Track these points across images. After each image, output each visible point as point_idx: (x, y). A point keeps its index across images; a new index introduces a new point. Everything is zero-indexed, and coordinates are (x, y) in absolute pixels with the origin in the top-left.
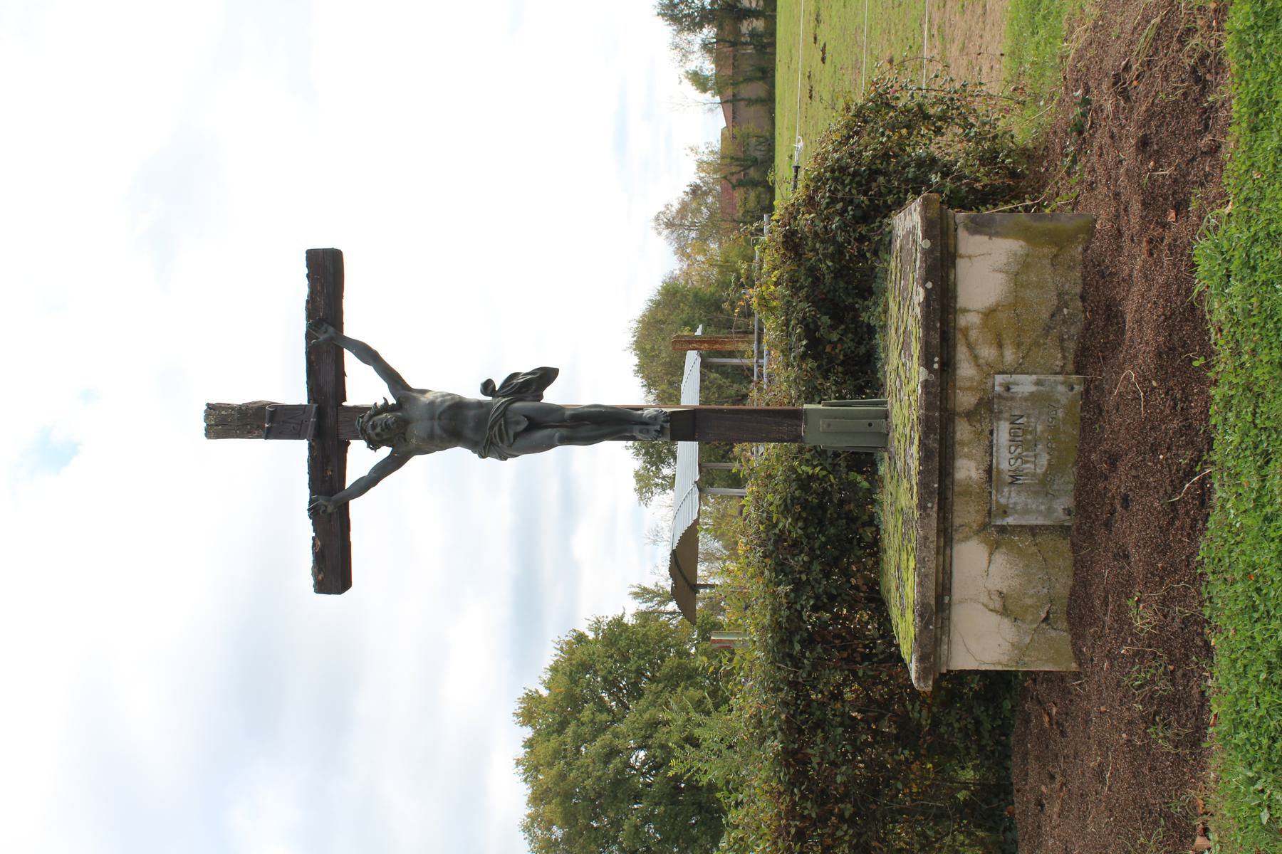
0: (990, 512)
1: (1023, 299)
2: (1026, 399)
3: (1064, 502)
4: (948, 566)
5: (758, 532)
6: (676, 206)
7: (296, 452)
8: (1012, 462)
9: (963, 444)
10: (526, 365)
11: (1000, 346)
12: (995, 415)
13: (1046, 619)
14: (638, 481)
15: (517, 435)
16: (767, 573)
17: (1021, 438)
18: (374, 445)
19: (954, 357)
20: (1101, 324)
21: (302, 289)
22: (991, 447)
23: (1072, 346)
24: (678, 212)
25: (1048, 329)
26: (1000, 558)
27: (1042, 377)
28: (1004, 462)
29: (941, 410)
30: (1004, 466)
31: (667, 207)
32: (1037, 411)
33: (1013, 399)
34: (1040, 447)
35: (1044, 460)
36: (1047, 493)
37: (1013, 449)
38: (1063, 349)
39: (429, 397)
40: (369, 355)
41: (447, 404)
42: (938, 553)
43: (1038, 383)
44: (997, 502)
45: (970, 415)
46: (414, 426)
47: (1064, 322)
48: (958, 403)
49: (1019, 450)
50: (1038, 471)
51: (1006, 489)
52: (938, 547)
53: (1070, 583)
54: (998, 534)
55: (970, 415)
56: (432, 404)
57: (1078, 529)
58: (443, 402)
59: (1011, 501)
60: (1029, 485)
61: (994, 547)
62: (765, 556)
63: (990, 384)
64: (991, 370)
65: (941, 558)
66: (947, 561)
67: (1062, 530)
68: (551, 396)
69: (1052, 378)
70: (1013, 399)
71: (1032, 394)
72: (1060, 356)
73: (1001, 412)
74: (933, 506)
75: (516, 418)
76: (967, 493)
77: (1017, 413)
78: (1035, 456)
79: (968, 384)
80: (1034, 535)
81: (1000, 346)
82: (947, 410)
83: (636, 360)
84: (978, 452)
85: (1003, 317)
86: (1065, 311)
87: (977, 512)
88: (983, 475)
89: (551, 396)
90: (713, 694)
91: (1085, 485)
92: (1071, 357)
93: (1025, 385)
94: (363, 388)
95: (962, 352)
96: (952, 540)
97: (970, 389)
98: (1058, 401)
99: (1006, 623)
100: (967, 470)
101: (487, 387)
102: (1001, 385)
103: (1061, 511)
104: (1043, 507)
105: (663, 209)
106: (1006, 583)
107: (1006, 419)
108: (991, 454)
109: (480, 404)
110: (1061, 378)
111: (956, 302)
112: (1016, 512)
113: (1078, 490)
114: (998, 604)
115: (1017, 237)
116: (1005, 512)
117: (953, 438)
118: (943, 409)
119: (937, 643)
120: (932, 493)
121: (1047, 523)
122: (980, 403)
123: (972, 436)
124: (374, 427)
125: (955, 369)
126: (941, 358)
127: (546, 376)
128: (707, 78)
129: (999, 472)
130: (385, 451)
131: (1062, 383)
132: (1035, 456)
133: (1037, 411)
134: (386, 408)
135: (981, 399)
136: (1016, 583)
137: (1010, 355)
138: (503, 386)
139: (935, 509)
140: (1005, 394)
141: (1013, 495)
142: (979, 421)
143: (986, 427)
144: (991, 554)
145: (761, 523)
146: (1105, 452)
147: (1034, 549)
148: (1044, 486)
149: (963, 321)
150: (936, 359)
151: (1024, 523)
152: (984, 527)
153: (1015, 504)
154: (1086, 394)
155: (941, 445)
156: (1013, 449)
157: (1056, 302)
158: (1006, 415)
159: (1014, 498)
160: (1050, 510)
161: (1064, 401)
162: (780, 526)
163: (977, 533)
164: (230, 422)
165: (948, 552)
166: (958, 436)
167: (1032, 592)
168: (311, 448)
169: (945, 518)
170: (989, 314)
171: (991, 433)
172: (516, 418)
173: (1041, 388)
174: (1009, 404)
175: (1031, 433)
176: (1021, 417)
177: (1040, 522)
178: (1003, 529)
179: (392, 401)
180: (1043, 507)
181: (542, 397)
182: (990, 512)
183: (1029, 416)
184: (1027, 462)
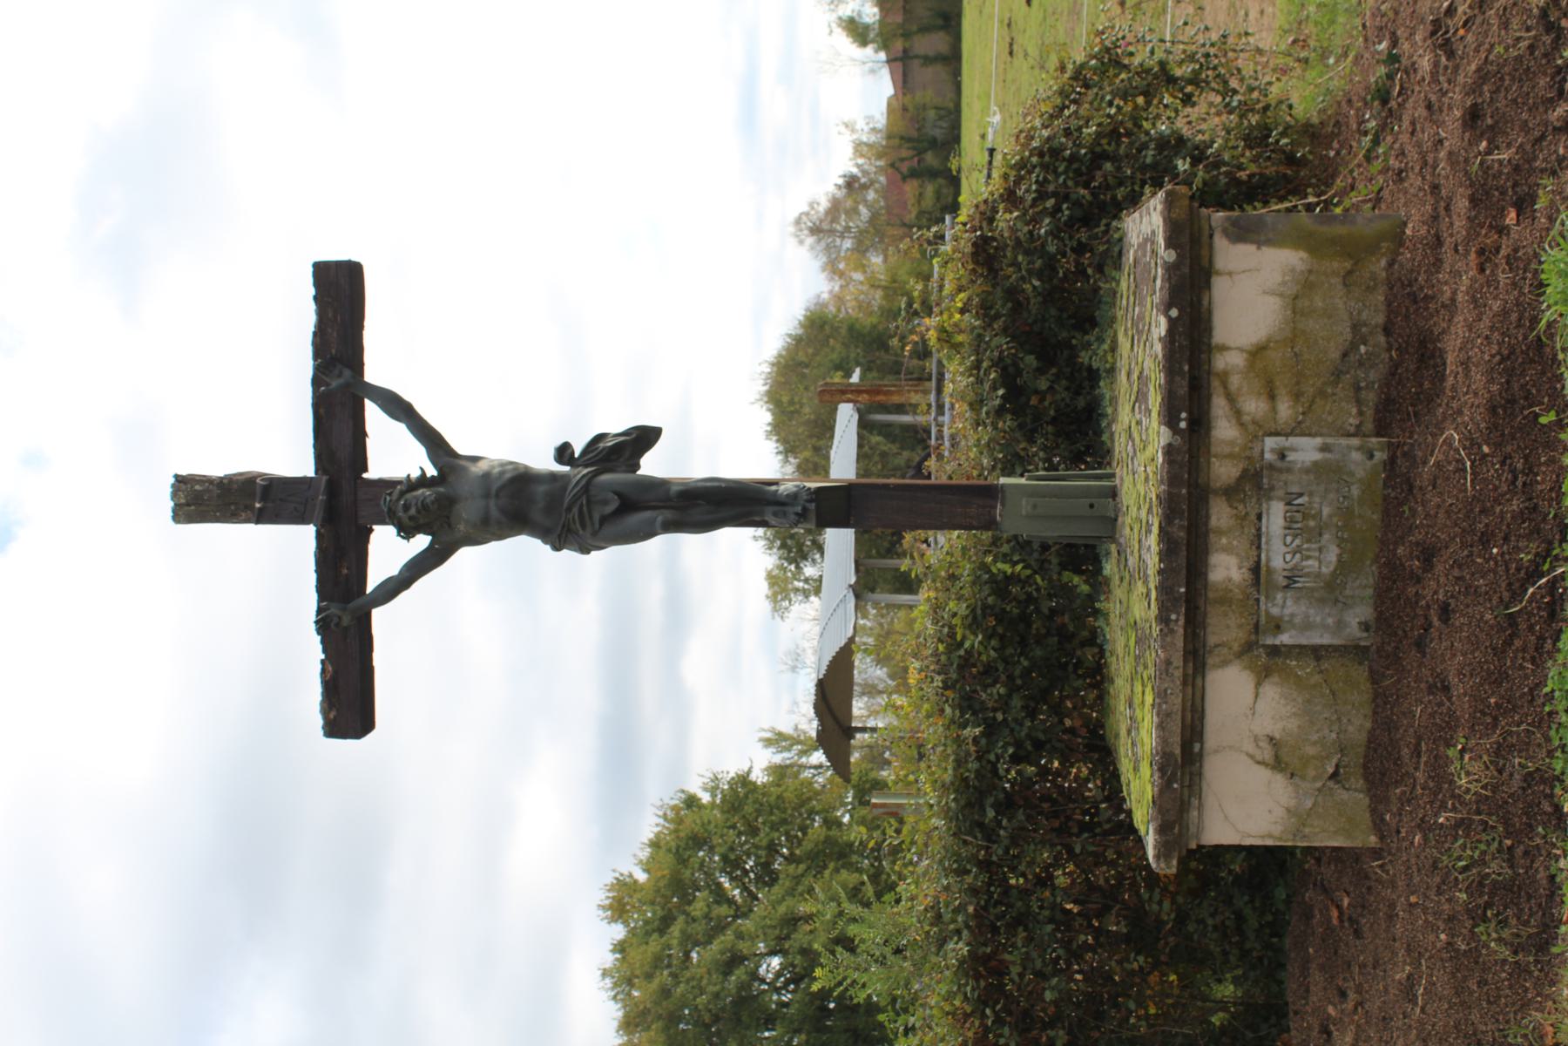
0: (1257, 626)
2: (1307, 471)
3: (1358, 615)
4: (1198, 701)
5: (936, 654)
6: (824, 204)
8: (1288, 557)
9: (1220, 532)
10: (616, 423)
11: (1272, 397)
14: (772, 585)
15: (604, 520)
16: (948, 710)
18: (407, 532)
19: (1208, 412)
20: (1412, 367)
21: (306, 316)
22: (1259, 536)
23: (1371, 397)
24: (828, 212)
25: (1337, 374)
26: (1271, 691)
27: (1329, 440)
28: (1278, 557)
29: (1189, 486)
30: (1277, 563)
31: (811, 205)
32: (1322, 487)
33: (1289, 470)
34: (1326, 536)
35: (1332, 555)
37: (1289, 539)
38: (1359, 402)
39: (482, 467)
40: (399, 408)
41: (508, 476)
42: (1184, 683)
43: (1325, 448)
44: (1267, 612)
45: (1231, 493)
46: (464, 505)
48: (1212, 476)
49: (1297, 542)
50: (1324, 570)
51: (1279, 596)
52: (1185, 675)
53: (1368, 725)
54: (1268, 658)
55: (1231, 493)
56: (486, 476)
57: (1378, 651)
58: (502, 473)
60: (1312, 590)
62: (946, 687)
63: (1257, 450)
64: (1258, 430)
66: (1198, 694)
68: (652, 465)
69: (1344, 441)
70: (1289, 470)
71: (1315, 463)
72: (1354, 411)
73: (1272, 488)
74: (1178, 619)
75: (602, 496)
76: (1225, 600)
77: (1295, 489)
78: (1320, 550)
79: (1227, 450)
80: (1318, 659)
81: (1272, 397)
83: (768, 417)
84: (1241, 543)
86: (1363, 349)
87: (1240, 626)
88: (1248, 575)
89: (652, 465)
91: (1389, 589)
92: (1369, 413)
93: (1306, 451)
94: (392, 454)
95: (1219, 405)
96: (1204, 665)
97: (1231, 456)
98: (1352, 474)
100: (1226, 568)
101: (563, 453)
102: (1272, 450)
105: (806, 209)
106: (1280, 726)
107: (1281, 499)
108: (1259, 547)
109: (553, 477)
110: (1355, 441)
112: (1294, 626)
117: (1206, 524)
121: (1336, 642)
122: (1244, 475)
123: (1232, 522)
124: (406, 507)
125: (1209, 429)
126: (1190, 413)
127: (645, 437)
128: (867, 27)
129: (1270, 571)
130: (422, 541)
131: (1359, 449)
132: (1320, 550)
133: (1322, 487)
134: (423, 481)
135: (1245, 471)
136: (1293, 725)
138: (585, 452)
139: (1182, 622)
140: (1279, 464)
141: (1289, 603)
142: (1243, 501)
144: (1258, 684)
145: (940, 641)
146: (1417, 544)
147: (1317, 678)
148: (1331, 591)
150: (1184, 415)
151: (1304, 642)
152: (1248, 648)
153: (1292, 615)
154: (1391, 463)
155: (1189, 533)
156: (1289, 539)
157: (1349, 337)
158: (1280, 493)
160: (1340, 625)
161: (1360, 473)
162: (967, 645)
163: (1239, 655)
164: (206, 500)
165: (1199, 681)
166: (1213, 522)
167: (1315, 737)
169: (1195, 635)
171: (1259, 517)
172: (602, 496)
173: (1328, 456)
174: (1284, 477)
175: (1314, 517)
176: (1301, 495)
177: (1326, 640)
178: (1274, 651)
179: (431, 471)
180: (1330, 621)
181: (638, 467)
182: (1257, 626)
184: (1308, 558)
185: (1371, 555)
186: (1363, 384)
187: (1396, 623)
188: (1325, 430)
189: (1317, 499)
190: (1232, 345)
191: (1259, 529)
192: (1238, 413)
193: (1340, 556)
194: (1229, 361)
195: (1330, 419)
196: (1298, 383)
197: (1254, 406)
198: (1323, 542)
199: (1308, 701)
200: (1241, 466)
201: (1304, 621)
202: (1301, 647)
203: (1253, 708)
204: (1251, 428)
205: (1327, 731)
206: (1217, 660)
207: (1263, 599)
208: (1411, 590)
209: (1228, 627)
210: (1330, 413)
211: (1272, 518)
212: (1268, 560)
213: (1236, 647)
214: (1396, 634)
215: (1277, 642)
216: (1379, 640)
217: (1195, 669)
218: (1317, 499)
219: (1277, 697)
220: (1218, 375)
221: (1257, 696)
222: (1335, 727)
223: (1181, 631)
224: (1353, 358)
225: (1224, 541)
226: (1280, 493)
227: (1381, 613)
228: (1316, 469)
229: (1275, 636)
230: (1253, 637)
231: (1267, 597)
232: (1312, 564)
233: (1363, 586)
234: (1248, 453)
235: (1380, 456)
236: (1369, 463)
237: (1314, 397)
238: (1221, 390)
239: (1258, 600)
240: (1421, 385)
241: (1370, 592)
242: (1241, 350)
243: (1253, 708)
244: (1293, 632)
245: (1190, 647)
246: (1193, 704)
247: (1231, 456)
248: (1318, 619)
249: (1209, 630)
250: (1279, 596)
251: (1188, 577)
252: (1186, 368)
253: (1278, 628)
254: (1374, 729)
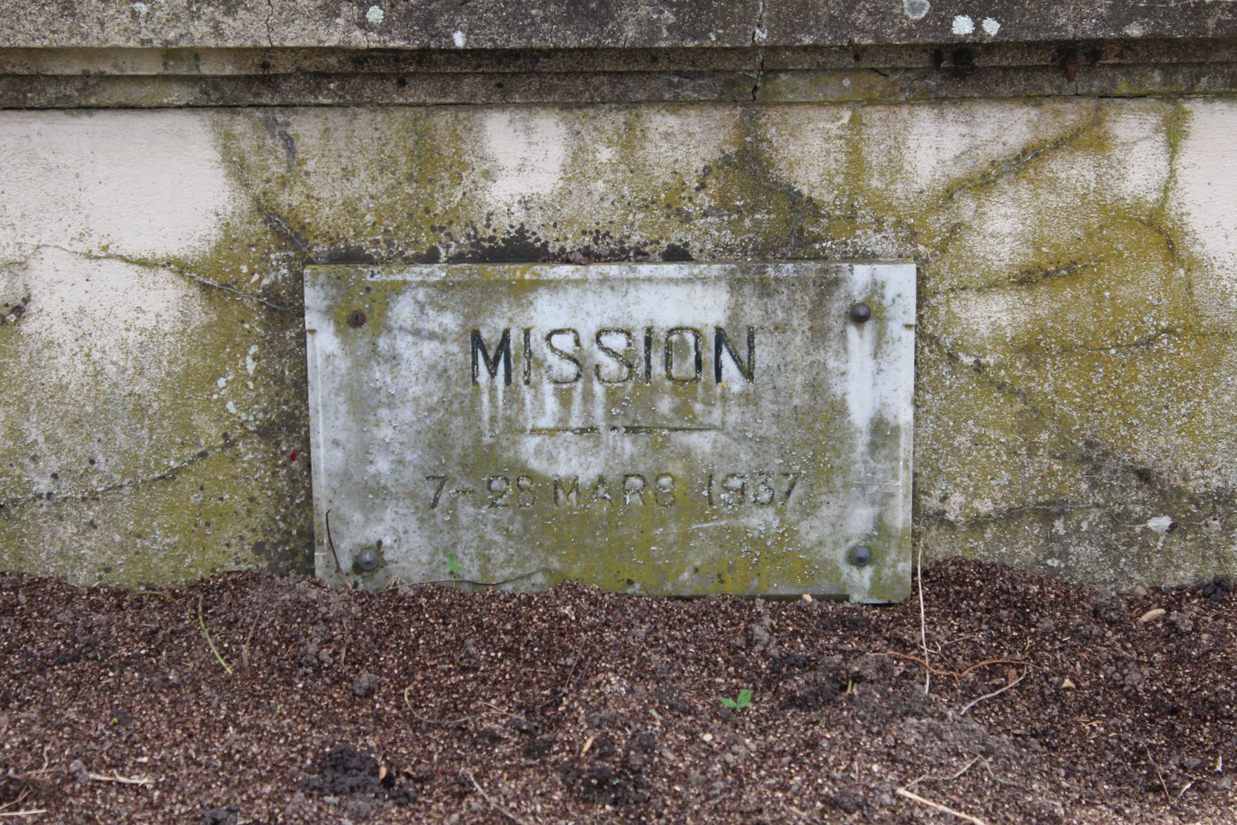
0: (353, 257)
1: (1215, 361)
2: (816, 387)
3: (409, 549)
4: (119, 94)
8: (564, 342)
9: (629, 141)
11: (1026, 278)
12: (751, 264)
19: (990, 97)
20: (1135, 678)
22: (619, 255)
23: (1023, 550)
25: (1091, 458)
26: (164, 303)
27: (905, 444)
28: (563, 311)
29: (772, 49)
30: (546, 312)
32: (769, 429)
33: (819, 335)
34: (627, 446)
35: (573, 463)
36: (442, 482)
37: (617, 342)
38: (1010, 517)
42: (169, 53)
43: (882, 432)
44: (398, 289)
45: (748, 167)
47: (1117, 520)
48: (795, 115)
49: (611, 366)
50: (530, 444)
51: (450, 321)
52: (196, 54)
53: (82, 578)
54: (265, 290)
55: (748, 167)
57: (304, 607)
59: (404, 345)
60: (471, 410)
61: (208, 278)
63: (873, 241)
64: (930, 236)
65: (156, 69)
66: (136, 94)
67: (296, 541)
69: (902, 484)
70: (819, 335)
71: (839, 409)
72: (985, 506)
73: (765, 290)
76: (428, 163)
77: (764, 355)
78: (588, 431)
79: (874, 156)
80: (266, 432)
81: (1026, 278)
82: (770, 72)
84: (598, 205)
85: (1144, 286)
86: (1161, 523)
87: (351, 207)
88: (503, 226)
90: (976, 487)
91: (486, 634)
92: (979, 548)
93: (875, 382)
95: (1005, 127)
96: (230, 107)
97: (856, 164)
98: (809, 509)
100: (523, 161)
102: (877, 287)
103: (373, 533)
104: (382, 465)
106: (61, 331)
107: (734, 317)
108: (589, 256)
110: (901, 516)
111: (1211, 96)
112: (359, 365)
113: (464, 602)
116: (357, 320)
117: (655, 101)
118: (772, 63)
120: (428, 21)
121: (321, 485)
122: (800, 206)
123: (662, 175)
125: (936, 100)
126: (992, 47)
129: (522, 291)
131: (880, 525)
132: (588, 431)
133: (769, 429)
135: (813, 208)
136: (67, 369)
137: (990, 316)
139: (360, 39)
140: (837, 306)
141: (430, 349)
142: (724, 205)
143: (701, 232)
144: (180, 267)
146: (647, 746)
147: (209, 432)
148: (468, 465)
149: (1134, 128)
150: (991, 27)
151: (317, 394)
152: (290, 235)
153: (394, 359)
154: (843, 619)
155: (629, 53)
156: (617, 342)
157: (1195, 486)
158: (753, 313)
160: (373, 495)
161: (811, 531)
163: (264, 210)
165: (177, 94)
166: (661, 122)
167: (34, 433)
169: (320, 78)
170: (1160, 232)
171: (677, 254)
173: (862, 443)
174: (800, 321)
175: (682, 410)
176: (748, 374)
177: (325, 458)
178: (284, 310)
180: (382, 465)
182: (353, 257)
183: (748, 399)
184: (565, 399)
185: (576, 570)
186: (1059, 526)
187: (389, 660)
188: (929, 428)
189: (734, 417)
190: (1184, 160)
191: (641, 255)
192: (982, 183)
193: (574, 485)
194: (1137, 152)
195: (962, 440)
196: (1067, 349)
197: (1002, 228)
198: (610, 437)
199: (140, 410)
200: (825, 196)
201: (377, 399)
202: (301, 385)
203: (107, 254)
204: (939, 223)
205: (54, 465)
206: (247, 145)
207: (438, 272)
208: (495, 714)
209: (348, 174)
210: (977, 441)
211: (679, 292)
212: (554, 286)
213: (289, 199)
214: (357, 662)
215: (311, 320)
216: (337, 604)
217: (215, 82)
218: (734, 417)
219: (148, 322)
220: (1098, 122)
221: (143, 263)
222: (66, 488)
223: (333, 39)
224: (1136, 497)
225: (605, 154)
226: (753, 313)
227: (413, 608)
228: (825, 411)
229: (328, 312)
230: (321, 248)
231: (443, 286)
232: (544, 407)
233: (489, 552)
234: (865, 215)
235: (861, 584)
236: (840, 555)
237: (1026, 396)
238: (1050, 132)
239: (431, 257)
240: (1087, 708)
241: (471, 570)
242: (1168, 186)
243: (107, 254)
244: (343, 364)
245: (282, 66)
246: (104, 78)
247: (856, 164)
248: (386, 433)
249: (337, 119)
250: (450, 321)
251: (1171, 44)
252: (1135, 31)
253: (353, 321)
254: (72, 595)
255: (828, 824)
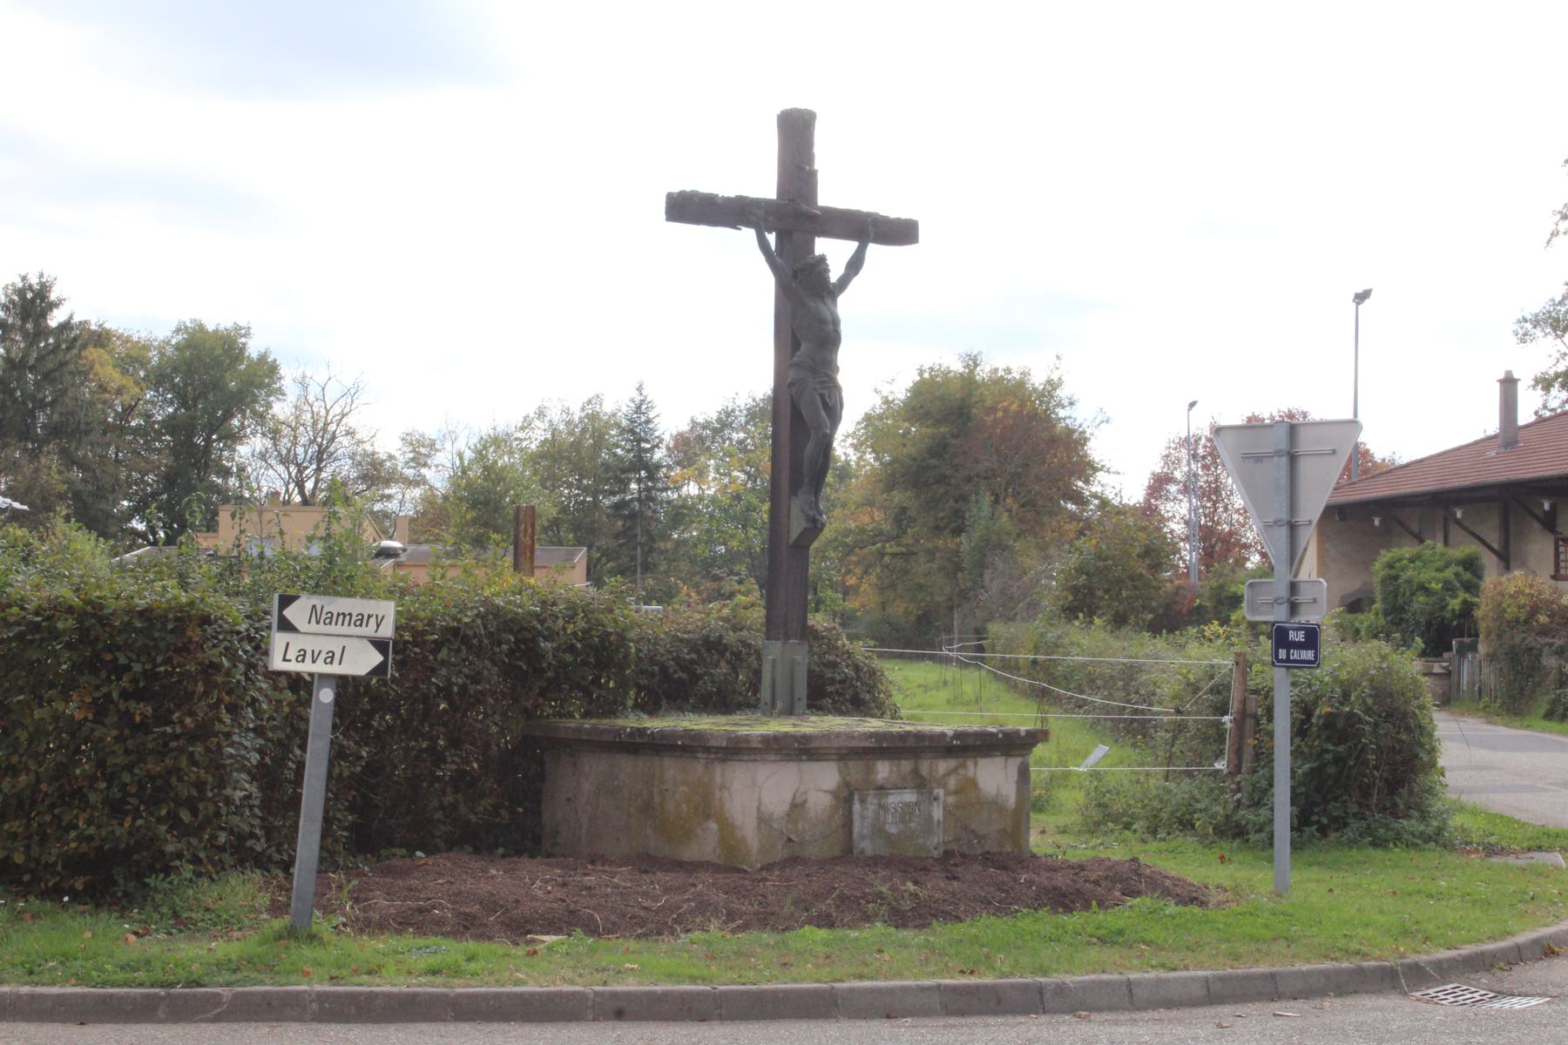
7: (763, 185)
9: (899, 766)
13: (790, 840)
17: (907, 811)
28: (893, 799)
30: (891, 799)
35: (893, 830)
45: (916, 772)
54: (845, 797)
55: (916, 772)
81: (956, 793)
95: (951, 763)
99: (785, 807)
100: (883, 770)
114: (799, 800)
115: (1017, 802)
119: (779, 751)
121: (855, 835)
127: (71, 317)
148: (878, 830)
149: (970, 763)
159: (871, 808)
160: (863, 837)
164: (796, 132)
166: (904, 762)
168: (767, 202)
170: (973, 783)
177: (856, 829)
197: (952, 782)
255: (1310, 1044)
